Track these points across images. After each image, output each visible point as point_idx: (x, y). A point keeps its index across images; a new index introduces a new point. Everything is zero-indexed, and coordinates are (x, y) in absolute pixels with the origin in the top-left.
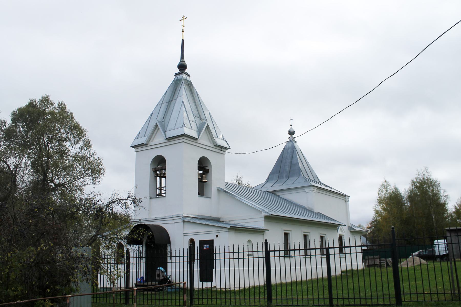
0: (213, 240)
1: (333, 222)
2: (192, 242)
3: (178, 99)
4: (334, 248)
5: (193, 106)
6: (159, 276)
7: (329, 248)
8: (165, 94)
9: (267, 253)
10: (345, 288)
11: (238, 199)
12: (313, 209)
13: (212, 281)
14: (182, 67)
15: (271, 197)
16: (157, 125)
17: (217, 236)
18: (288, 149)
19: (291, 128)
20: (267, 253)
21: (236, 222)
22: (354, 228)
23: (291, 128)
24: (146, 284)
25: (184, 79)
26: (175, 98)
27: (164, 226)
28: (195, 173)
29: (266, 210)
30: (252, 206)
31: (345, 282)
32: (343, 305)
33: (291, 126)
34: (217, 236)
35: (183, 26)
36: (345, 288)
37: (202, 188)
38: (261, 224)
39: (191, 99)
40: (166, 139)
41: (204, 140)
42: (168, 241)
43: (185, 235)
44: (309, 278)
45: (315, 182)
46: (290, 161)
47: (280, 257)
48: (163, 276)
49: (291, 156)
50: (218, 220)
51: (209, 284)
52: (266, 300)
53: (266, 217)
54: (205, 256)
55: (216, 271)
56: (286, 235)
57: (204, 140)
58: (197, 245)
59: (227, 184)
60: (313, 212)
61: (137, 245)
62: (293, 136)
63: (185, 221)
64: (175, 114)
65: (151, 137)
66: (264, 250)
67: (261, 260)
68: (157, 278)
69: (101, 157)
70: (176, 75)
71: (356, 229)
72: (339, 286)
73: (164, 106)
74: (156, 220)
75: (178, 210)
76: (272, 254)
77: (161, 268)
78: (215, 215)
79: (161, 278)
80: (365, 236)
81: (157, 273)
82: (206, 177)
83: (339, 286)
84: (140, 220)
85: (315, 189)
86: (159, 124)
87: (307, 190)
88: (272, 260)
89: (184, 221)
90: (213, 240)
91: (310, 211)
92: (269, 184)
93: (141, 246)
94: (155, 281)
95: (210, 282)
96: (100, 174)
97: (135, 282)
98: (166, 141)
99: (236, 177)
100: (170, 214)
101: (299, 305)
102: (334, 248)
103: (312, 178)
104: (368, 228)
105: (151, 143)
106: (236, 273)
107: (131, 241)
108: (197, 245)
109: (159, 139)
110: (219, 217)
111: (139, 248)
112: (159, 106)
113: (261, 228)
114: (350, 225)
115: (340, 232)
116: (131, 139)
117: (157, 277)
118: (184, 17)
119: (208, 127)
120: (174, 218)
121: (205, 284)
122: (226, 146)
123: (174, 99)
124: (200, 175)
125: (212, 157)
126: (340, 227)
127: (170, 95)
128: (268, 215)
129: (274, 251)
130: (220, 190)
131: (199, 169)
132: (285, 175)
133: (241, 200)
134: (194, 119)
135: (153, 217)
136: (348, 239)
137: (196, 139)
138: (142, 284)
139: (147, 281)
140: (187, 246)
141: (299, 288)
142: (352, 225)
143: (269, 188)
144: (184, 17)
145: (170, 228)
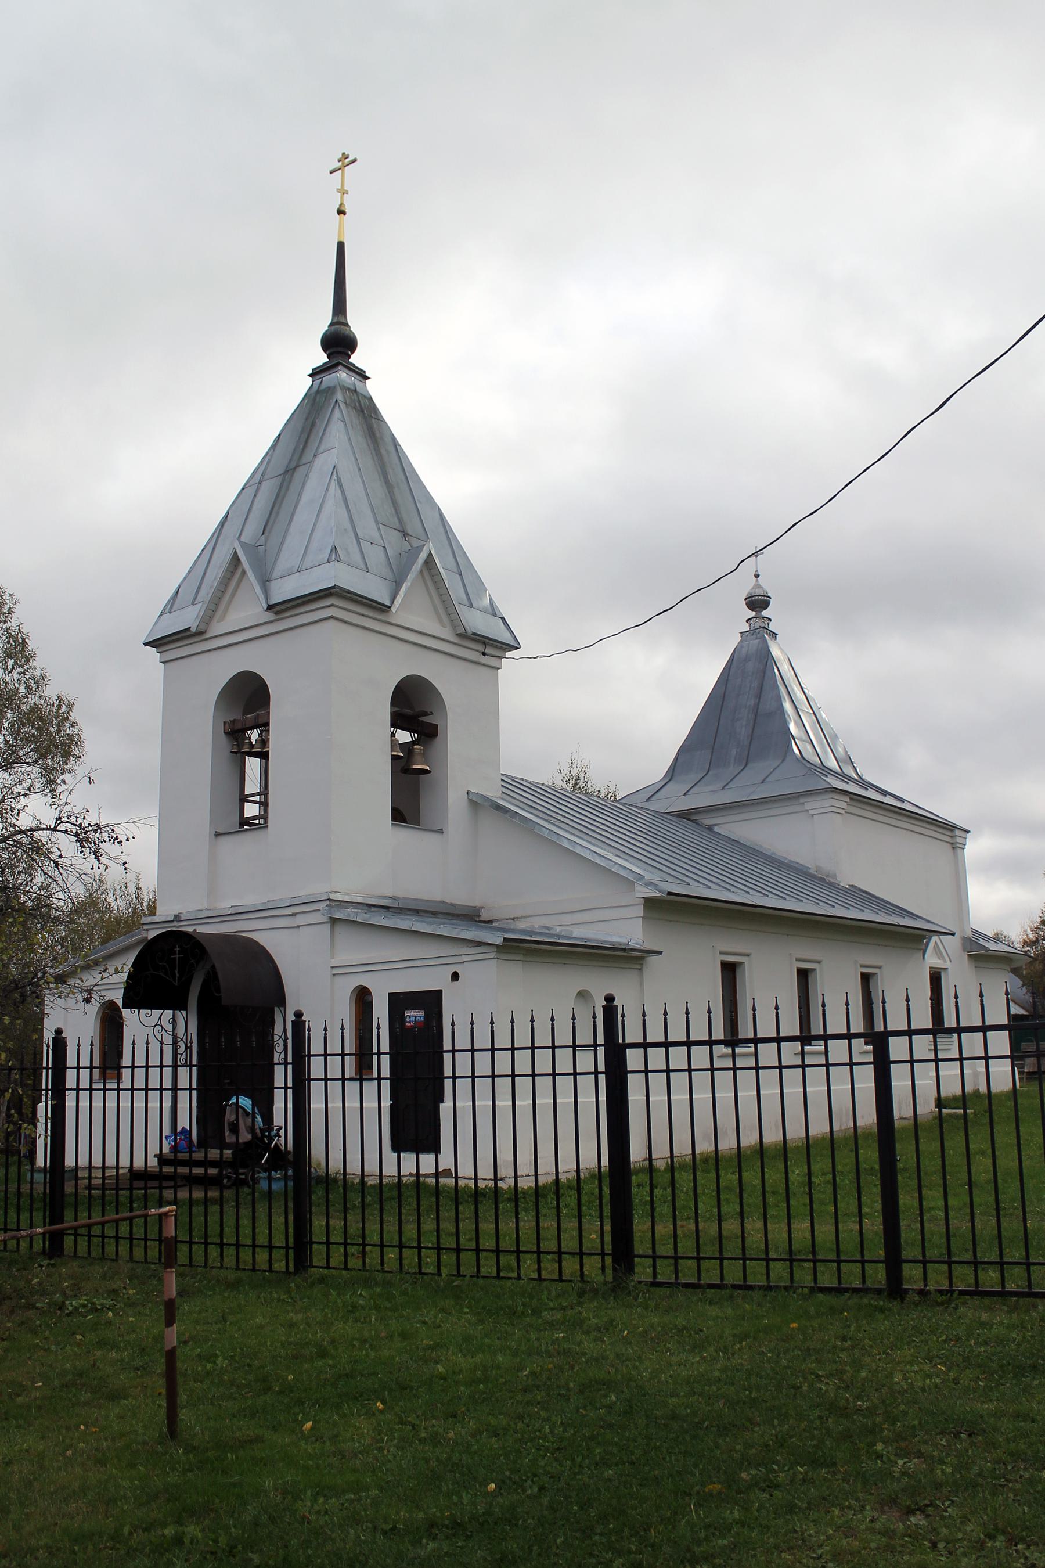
0: (439, 993)
1: (907, 922)
2: (363, 998)
3: (319, 462)
4: (910, 1033)
5: (378, 490)
6: (235, 1129)
7: (887, 1034)
8: (274, 447)
9: (616, 1053)
10: (958, 1177)
11: (546, 833)
12: (835, 876)
13: (434, 1147)
14: (339, 344)
15: (682, 831)
16: (236, 560)
17: (455, 976)
18: (747, 659)
19: (758, 586)
20: (616, 1053)
21: (537, 923)
22: (982, 942)
23: (758, 586)
24: (199, 1156)
25: (345, 388)
26: (308, 456)
27: (263, 939)
28: (376, 739)
29: (648, 876)
30: (598, 861)
31: (955, 1144)
32: (951, 1292)
33: (757, 576)
34: (455, 976)
35: (343, 192)
36: (958, 1177)
37: (410, 795)
38: (629, 930)
39: (368, 462)
40: (270, 608)
41: (413, 611)
42: (275, 992)
43: (337, 972)
44: (819, 1127)
45: (846, 778)
46: (752, 702)
47: (668, 1071)
48: (252, 1129)
49: (755, 684)
50: (471, 916)
51: (427, 1161)
52: (609, 1260)
53: (651, 904)
54: (415, 1056)
55: (455, 1108)
56: (730, 971)
57: (413, 611)
58: (381, 1013)
59: (510, 783)
60: (833, 886)
61: (163, 1007)
62: (764, 613)
63: (341, 917)
64: (303, 516)
65: (214, 608)
66: (601, 1040)
67: (586, 1083)
68: (229, 1138)
69: (69, 694)
70: (315, 373)
71: (992, 946)
72: (931, 1165)
73: (268, 488)
74: (236, 914)
75: (318, 879)
76: (634, 1059)
77: (246, 1102)
78: (460, 896)
79: (245, 1137)
80: (1015, 971)
81: (230, 1116)
82: (424, 754)
83: (931, 1165)
84: (177, 918)
85: (843, 803)
86: (243, 554)
87: (812, 805)
88: (634, 1084)
89: (334, 921)
90: (439, 993)
91: (824, 882)
92: (676, 788)
93: (181, 1016)
94: (222, 1145)
95: (427, 1151)
96: (67, 755)
97: (154, 1149)
98: (270, 616)
99: (566, 769)
100: (281, 894)
101: (751, 1288)
102: (910, 1033)
103: (832, 764)
104: (1025, 943)
105: (217, 628)
106: (518, 1127)
107: (142, 992)
108: (381, 1013)
109: (246, 609)
110: (477, 904)
111: (174, 1022)
112: (251, 491)
113: (633, 944)
114: (969, 934)
115: (932, 960)
116: (147, 617)
117: (227, 1133)
118: (345, 156)
119: (429, 561)
120: (299, 905)
121: (408, 1160)
122: (506, 638)
123: (304, 460)
124: (407, 747)
125: (450, 681)
126: (935, 938)
127: (292, 447)
128: (656, 894)
129: (645, 1045)
130: (477, 804)
131: (398, 721)
132: (734, 752)
133: (555, 839)
134: (375, 534)
135: (225, 905)
136: (962, 980)
137: (385, 609)
138: (183, 1156)
139: (203, 1143)
140: (345, 1012)
141: (774, 1176)
142: (974, 931)
143: (676, 800)
144: (345, 156)
145: (283, 946)
